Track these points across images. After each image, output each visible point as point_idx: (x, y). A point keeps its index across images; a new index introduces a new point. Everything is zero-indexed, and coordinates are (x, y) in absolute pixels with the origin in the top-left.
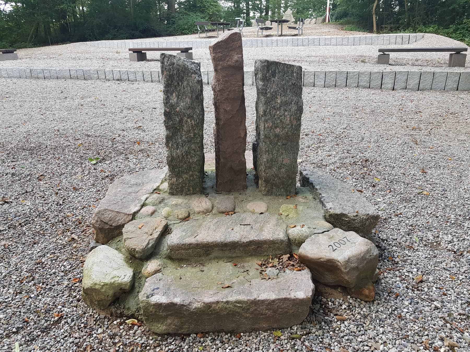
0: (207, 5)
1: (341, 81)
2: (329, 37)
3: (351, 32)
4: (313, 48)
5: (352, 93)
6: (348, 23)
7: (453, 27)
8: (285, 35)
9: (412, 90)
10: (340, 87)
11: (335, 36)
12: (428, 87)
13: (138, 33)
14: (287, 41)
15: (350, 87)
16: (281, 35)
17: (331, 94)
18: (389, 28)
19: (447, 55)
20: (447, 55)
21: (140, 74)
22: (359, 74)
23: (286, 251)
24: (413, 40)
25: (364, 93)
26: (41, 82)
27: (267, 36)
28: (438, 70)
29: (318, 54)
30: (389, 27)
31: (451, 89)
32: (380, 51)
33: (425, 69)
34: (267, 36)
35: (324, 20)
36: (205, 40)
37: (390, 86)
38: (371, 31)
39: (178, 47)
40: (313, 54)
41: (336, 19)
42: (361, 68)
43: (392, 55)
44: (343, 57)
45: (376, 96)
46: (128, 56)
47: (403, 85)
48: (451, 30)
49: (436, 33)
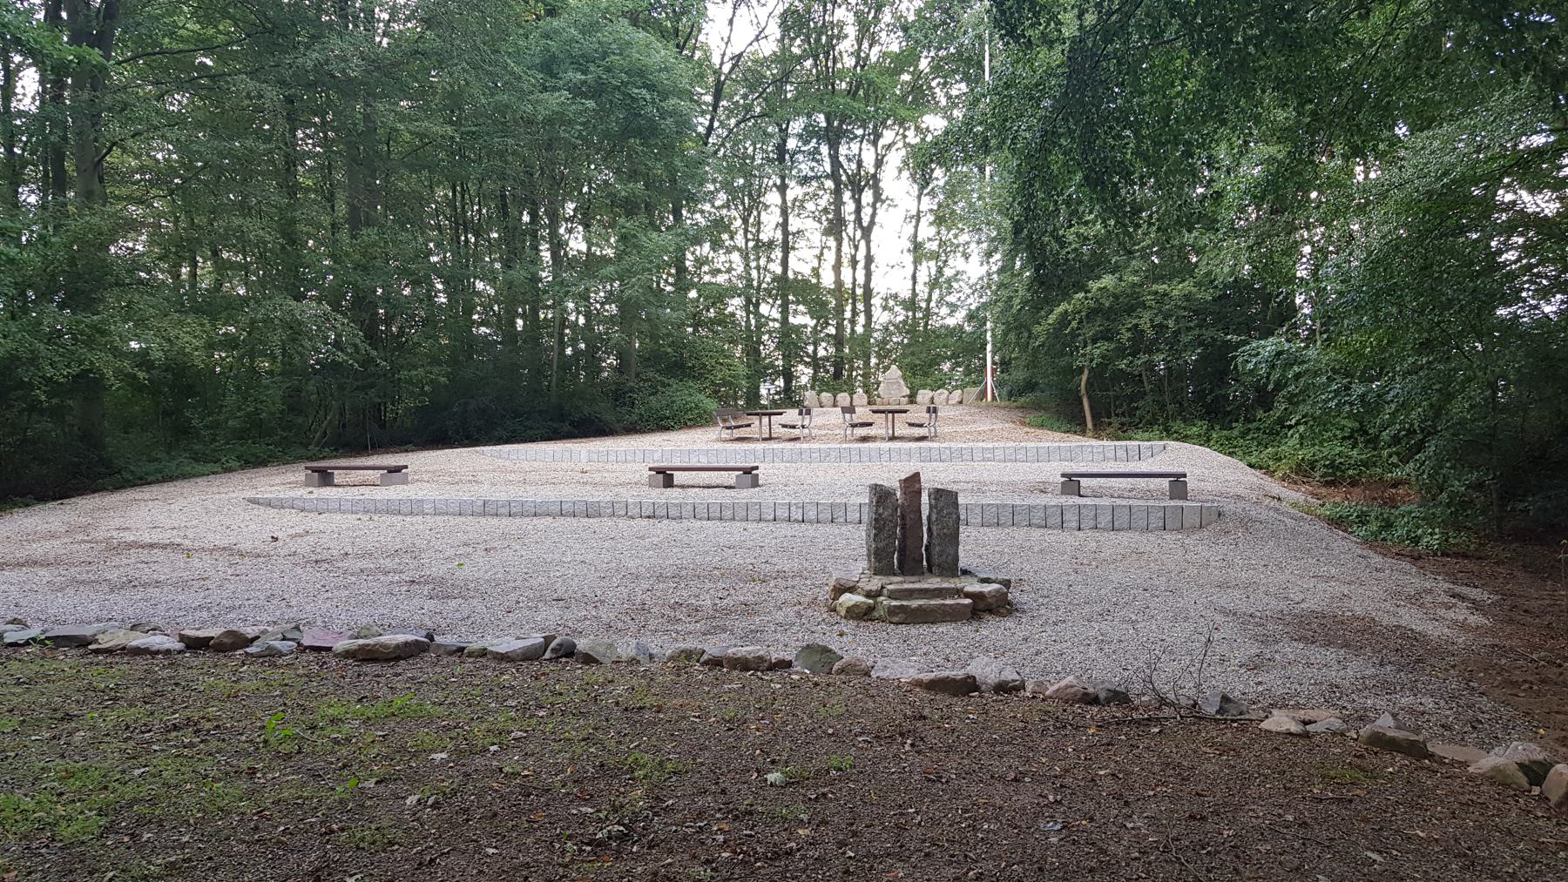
0: (709, 363)
1: (1006, 517)
2: (990, 446)
3: (1039, 432)
4: (959, 466)
5: (1020, 534)
6: (1037, 407)
7: (1238, 427)
8: (901, 438)
9: (1104, 529)
10: (1004, 525)
11: (1002, 445)
12: (1126, 526)
13: (567, 428)
14: (909, 453)
15: (1019, 526)
16: (893, 438)
17: (991, 534)
18: (1117, 425)
19: (1165, 483)
20: (1165, 482)
21: (690, 508)
22: (1030, 508)
23: (959, 592)
24: (1146, 453)
25: (1036, 533)
26: (518, 520)
27: (864, 439)
28: (1119, 502)
29: (971, 478)
30: (1115, 421)
31: (1157, 529)
32: (1063, 475)
33: (1119, 502)
34: (864, 439)
35: (983, 394)
36: (729, 446)
37: (1075, 525)
38: (1083, 433)
39: (739, 465)
40: (962, 477)
41: (1010, 394)
42: (1042, 500)
43: (1084, 482)
44: (1013, 483)
45: (1052, 537)
46: (645, 479)
47: (1092, 523)
48: (1236, 433)
49: (1205, 441)
